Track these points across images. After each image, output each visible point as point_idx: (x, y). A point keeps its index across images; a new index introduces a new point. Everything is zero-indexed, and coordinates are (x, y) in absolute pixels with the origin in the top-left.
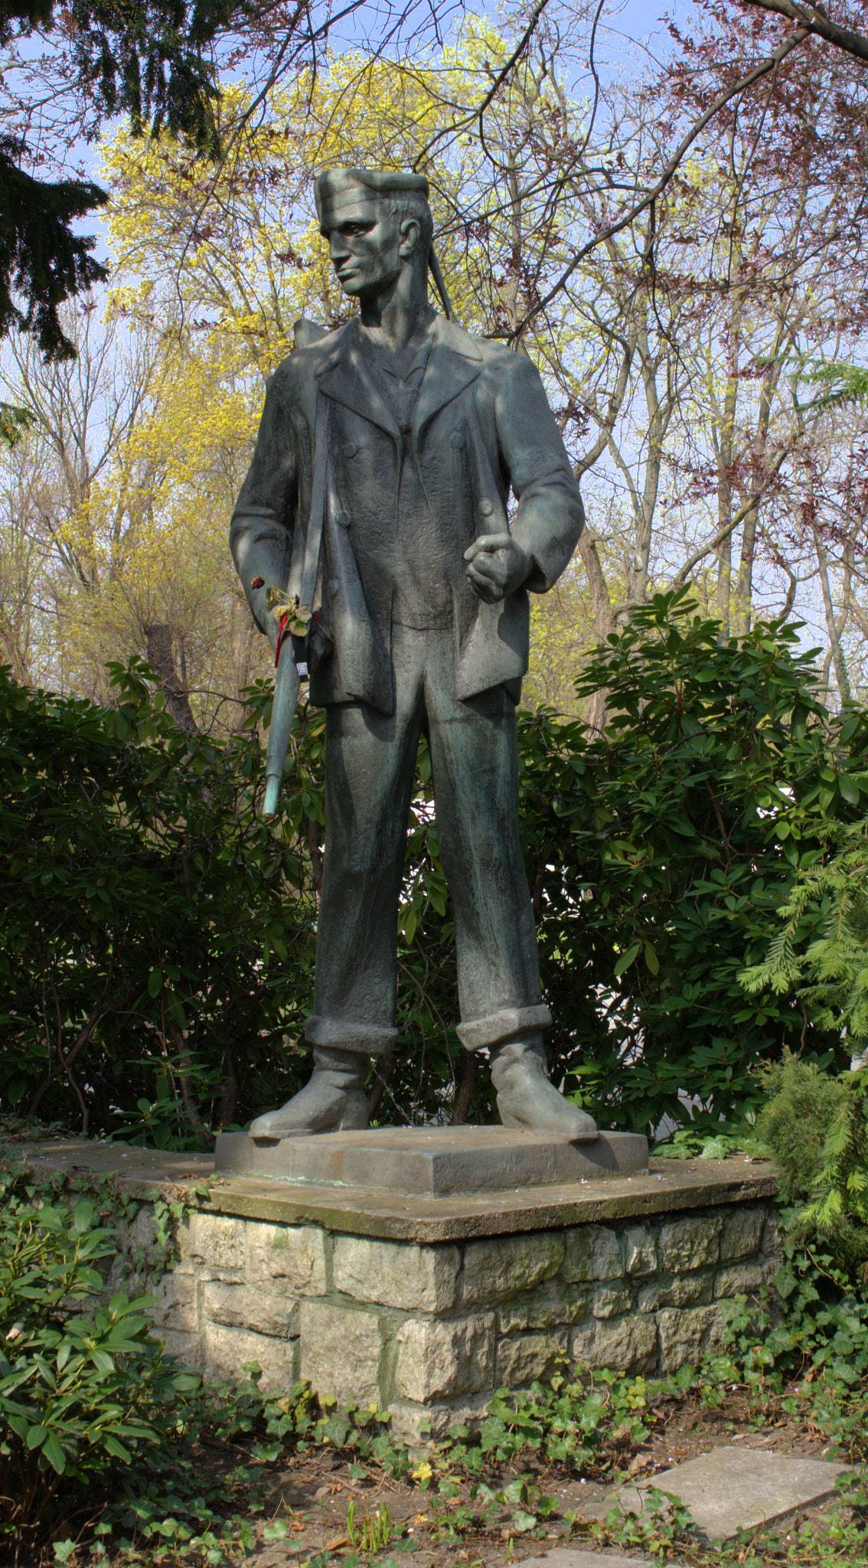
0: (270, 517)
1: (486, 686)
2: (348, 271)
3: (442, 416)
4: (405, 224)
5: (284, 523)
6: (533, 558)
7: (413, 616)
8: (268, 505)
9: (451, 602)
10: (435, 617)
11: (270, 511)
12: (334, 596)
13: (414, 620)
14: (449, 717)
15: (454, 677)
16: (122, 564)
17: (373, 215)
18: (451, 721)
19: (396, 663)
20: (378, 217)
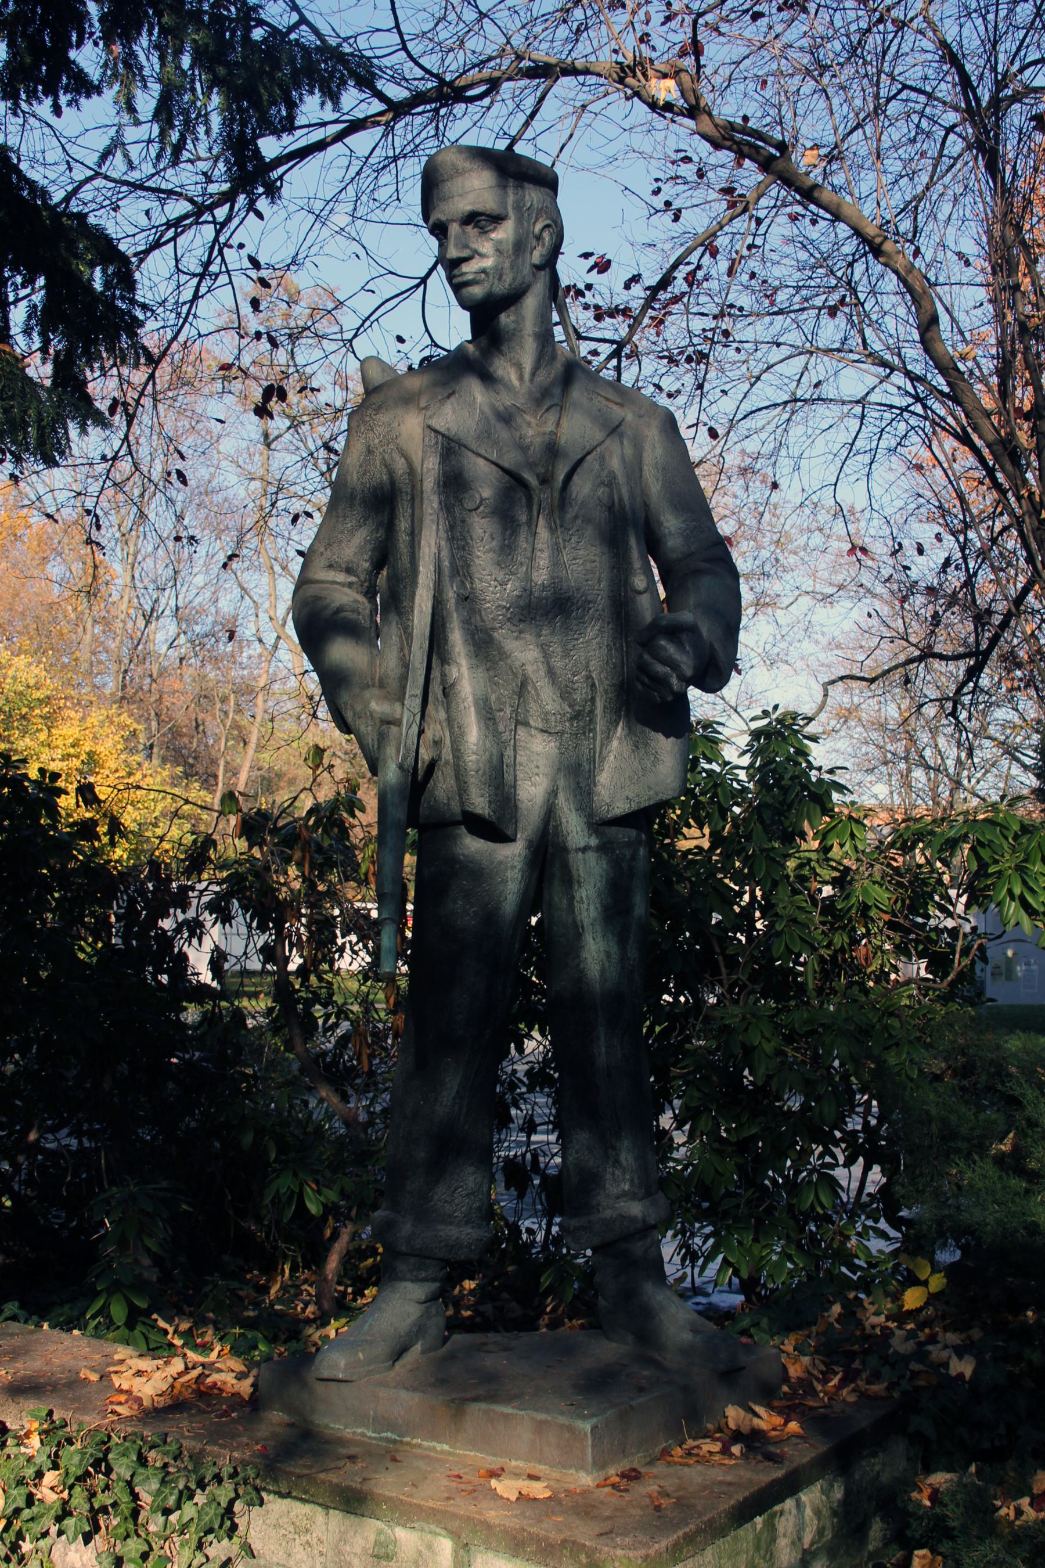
0: (350, 585)
1: (634, 807)
2: (470, 277)
3: (586, 465)
4: (538, 227)
5: (366, 594)
6: (711, 645)
7: (545, 717)
8: (349, 571)
9: (593, 700)
10: (571, 719)
11: (353, 579)
12: (453, 685)
13: (547, 721)
14: (582, 844)
15: (589, 794)
16: (71, 1443)
17: (506, 208)
18: (585, 849)
19: (520, 775)
20: (511, 213)
